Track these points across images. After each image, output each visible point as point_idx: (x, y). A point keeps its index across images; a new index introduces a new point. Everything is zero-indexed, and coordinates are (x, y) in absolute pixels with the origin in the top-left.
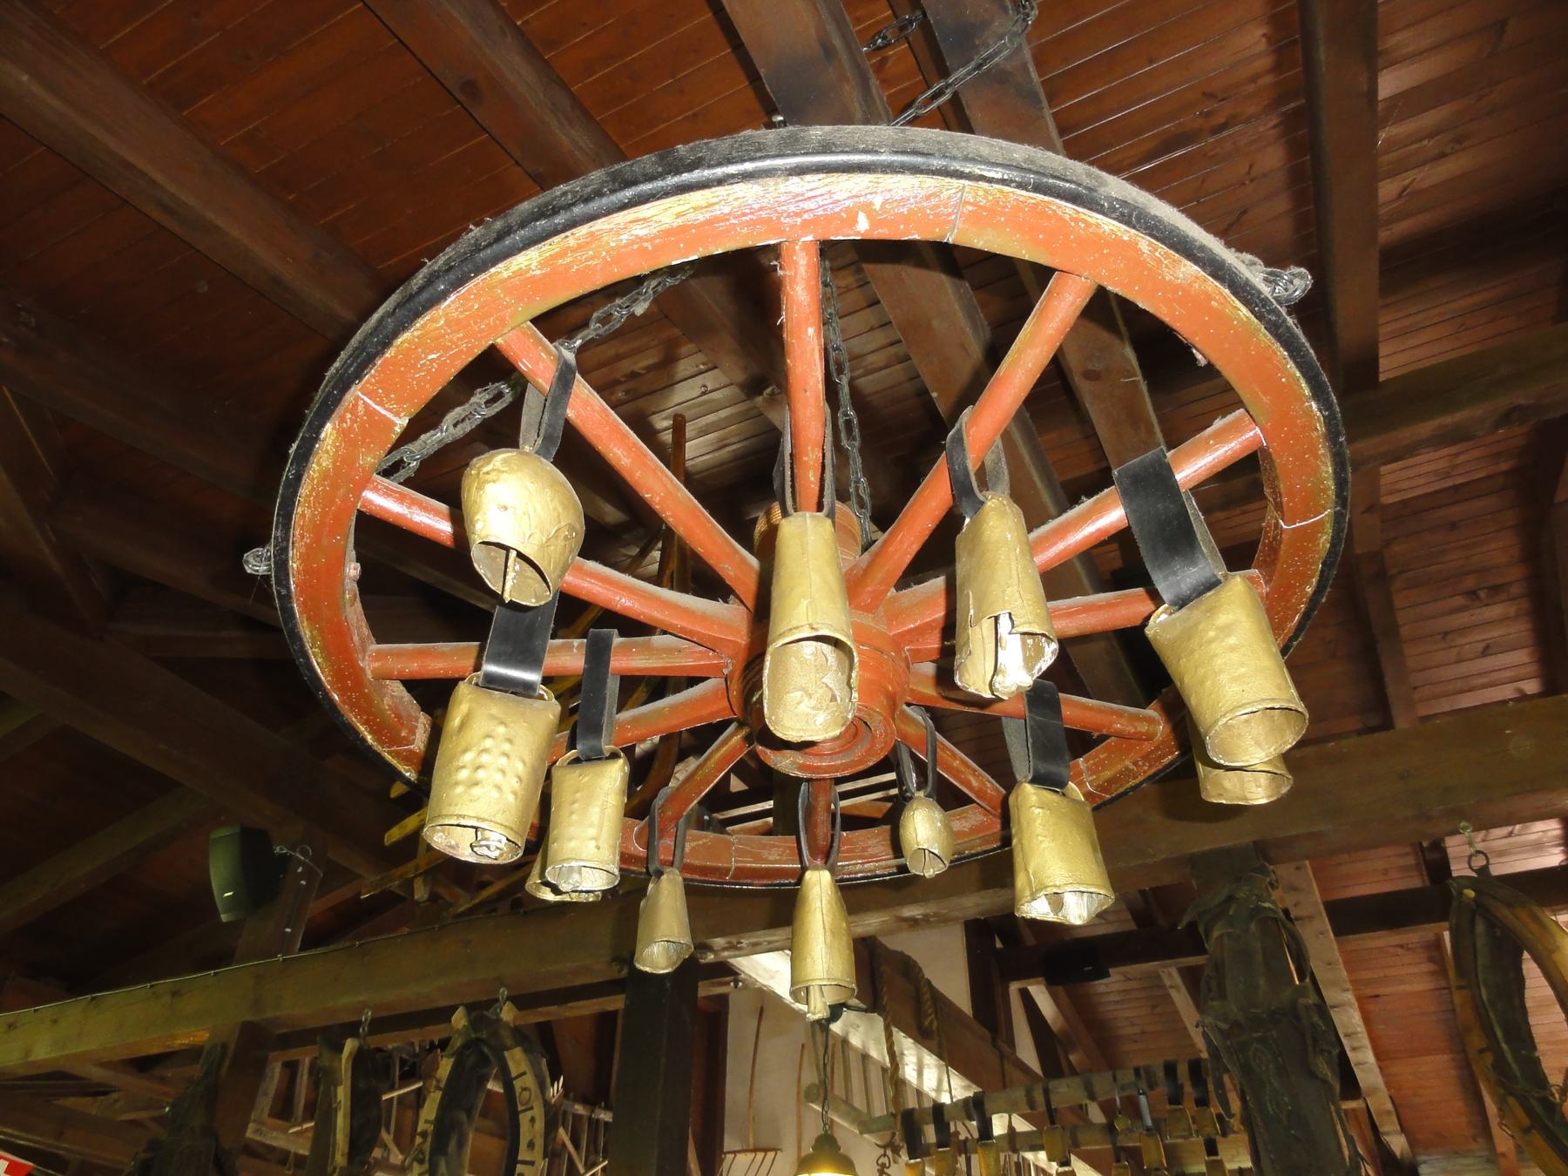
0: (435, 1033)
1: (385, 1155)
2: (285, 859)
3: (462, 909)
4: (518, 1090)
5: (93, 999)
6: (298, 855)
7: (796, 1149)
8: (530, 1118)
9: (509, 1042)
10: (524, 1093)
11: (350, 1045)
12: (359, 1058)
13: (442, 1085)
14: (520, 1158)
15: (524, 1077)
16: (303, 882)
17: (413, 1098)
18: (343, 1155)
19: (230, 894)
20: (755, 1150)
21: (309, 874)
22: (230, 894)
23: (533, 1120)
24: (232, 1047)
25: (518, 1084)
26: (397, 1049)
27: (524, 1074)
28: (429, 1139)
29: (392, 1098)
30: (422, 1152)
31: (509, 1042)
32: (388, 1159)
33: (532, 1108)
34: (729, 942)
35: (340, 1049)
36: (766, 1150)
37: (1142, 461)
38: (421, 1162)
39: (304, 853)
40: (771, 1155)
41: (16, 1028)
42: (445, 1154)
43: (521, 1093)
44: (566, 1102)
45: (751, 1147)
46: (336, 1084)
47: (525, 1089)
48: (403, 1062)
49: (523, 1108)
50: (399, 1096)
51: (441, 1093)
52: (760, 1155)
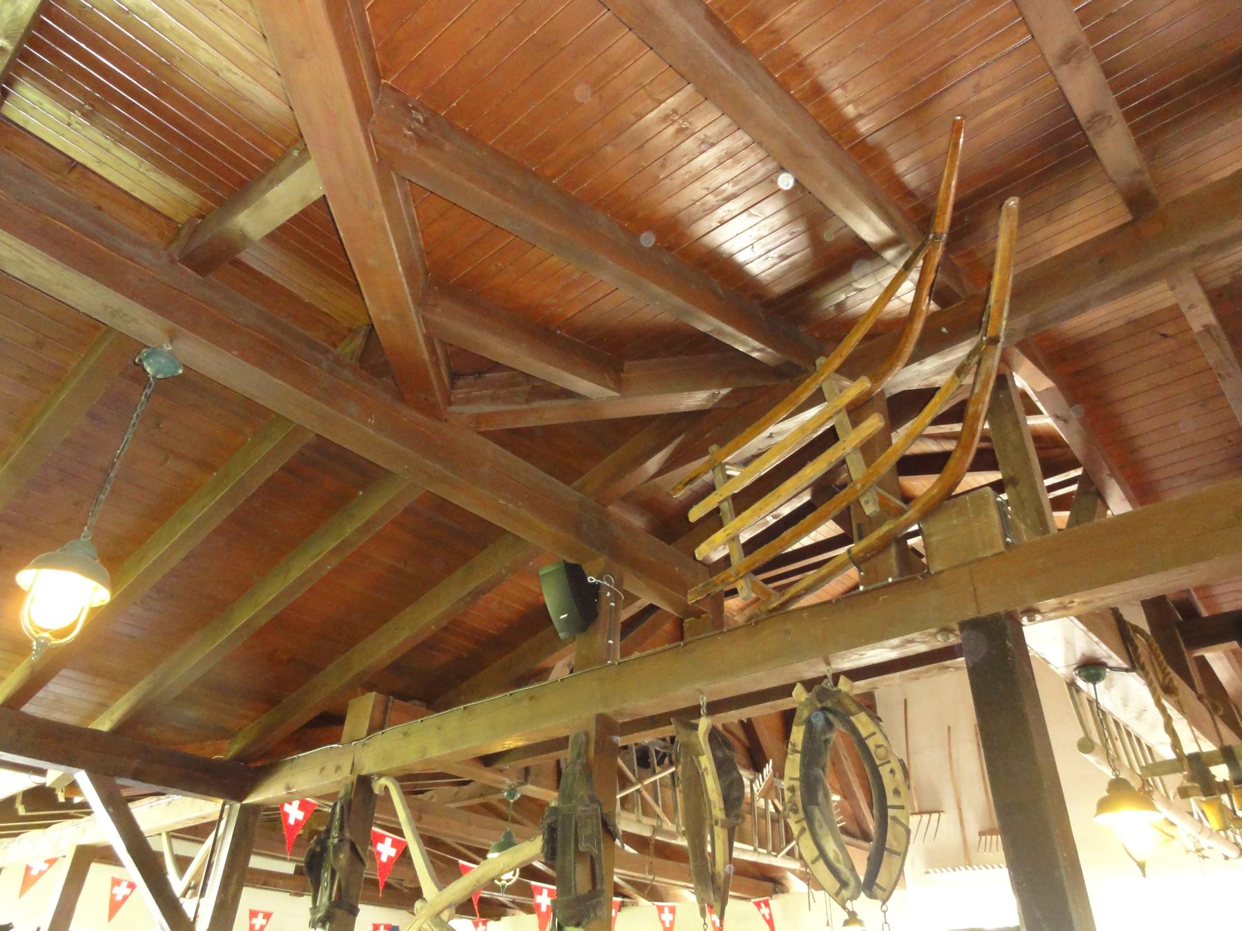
0: (784, 704)
1: (659, 824)
2: (596, 587)
3: (774, 605)
4: (872, 748)
5: (422, 721)
6: (605, 583)
7: (956, 811)
8: (889, 770)
9: (853, 708)
10: (879, 750)
11: (704, 723)
12: (713, 735)
13: (799, 748)
14: (889, 803)
15: (875, 736)
16: (613, 604)
17: (669, 781)
18: (720, 809)
19: (566, 615)
20: (921, 813)
21: (615, 596)
22: (566, 615)
23: (892, 771)
24: (593, 734)
25: (871, 743)
26: (652, 743)
27: (874, 733)
28: (798, 793)
29: (655, 781)
30: (795, 804)
31: (853, 708)
32: (661, 826)
33: (889, 762)
34: (1060, 603)
35: (695, 727)
36: (930, 813)
37: (410, 310)
38: (796, 812)
39: (608, 580)
40: (935, 816)
41: (409, 735)
42: (817, 804)
43: (876, 751)
44: (775, 780)
45: (917, 811)
46: (699, 754)
47: (878, 746)
48: (657, 752)
49: (881, 762)
50: (660, 779)
51: (799, 755)
52: (926, 817)
